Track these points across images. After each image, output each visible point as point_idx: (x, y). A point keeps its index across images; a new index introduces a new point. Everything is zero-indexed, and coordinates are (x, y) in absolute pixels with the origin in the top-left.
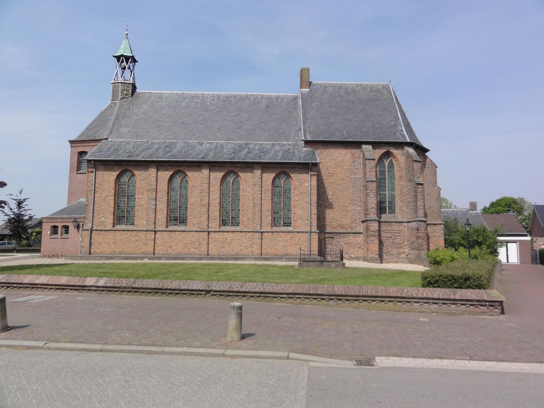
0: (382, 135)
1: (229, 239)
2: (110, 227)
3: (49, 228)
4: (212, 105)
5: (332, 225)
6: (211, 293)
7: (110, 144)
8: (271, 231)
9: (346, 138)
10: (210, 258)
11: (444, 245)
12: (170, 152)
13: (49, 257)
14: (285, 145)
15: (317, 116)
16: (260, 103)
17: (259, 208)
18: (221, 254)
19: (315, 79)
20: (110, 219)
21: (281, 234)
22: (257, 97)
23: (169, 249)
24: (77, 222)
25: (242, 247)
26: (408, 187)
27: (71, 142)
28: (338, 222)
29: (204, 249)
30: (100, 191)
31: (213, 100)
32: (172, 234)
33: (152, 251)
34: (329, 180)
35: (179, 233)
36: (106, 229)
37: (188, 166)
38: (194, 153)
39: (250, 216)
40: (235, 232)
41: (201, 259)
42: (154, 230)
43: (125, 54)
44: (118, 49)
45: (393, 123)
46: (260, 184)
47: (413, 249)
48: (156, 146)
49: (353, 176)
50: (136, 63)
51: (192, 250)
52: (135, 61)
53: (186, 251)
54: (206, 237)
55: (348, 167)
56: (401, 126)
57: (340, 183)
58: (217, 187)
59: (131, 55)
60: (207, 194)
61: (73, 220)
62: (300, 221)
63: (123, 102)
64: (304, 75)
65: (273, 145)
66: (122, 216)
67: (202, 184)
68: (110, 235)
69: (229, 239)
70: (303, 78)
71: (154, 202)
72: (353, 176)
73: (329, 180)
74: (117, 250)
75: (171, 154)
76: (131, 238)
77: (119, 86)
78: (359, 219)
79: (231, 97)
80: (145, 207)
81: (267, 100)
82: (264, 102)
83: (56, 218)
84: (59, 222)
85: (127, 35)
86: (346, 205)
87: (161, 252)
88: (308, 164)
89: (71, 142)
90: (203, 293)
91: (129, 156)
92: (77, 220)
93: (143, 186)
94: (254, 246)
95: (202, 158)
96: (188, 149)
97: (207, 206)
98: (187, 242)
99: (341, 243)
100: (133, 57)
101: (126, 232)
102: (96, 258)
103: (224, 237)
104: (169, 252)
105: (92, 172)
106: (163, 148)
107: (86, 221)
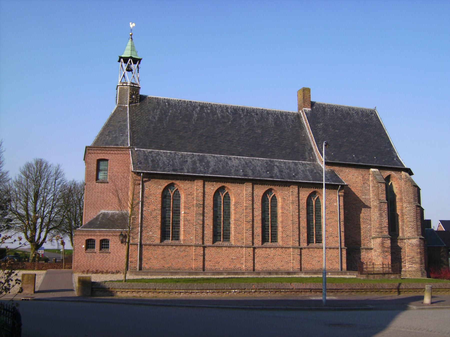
1: (272, 255)
2: (158, 241)
3: (84, 242)
8: (307, 247)
10: (256, 273)
11: (110, 243)
13: (113, 273)
15: (208, 109)
17: (297, 225)
18: (265, 269)
20: (157, 234)
22: (262, 112)
23: (217, 265)
25: (283, 263)
26: (407, 209)
29: (297, 266)
32: (219, 250)
33: (202, 267)
36: (154, 243)
40: (277, 248)
41: (196, 273)
42: (202, 245)
44: (124, 50)
46: (297, 202)
47: (413, 263)
49: (364, 197)
53: (232, 267)
54: (252, 253)
58: (259, 204)
60: (251, 211)
61: (119, 234)
62: (331, 238)
64: (306, 92)
68: (160, 250)
69: (272, 255)
71: (201, 218)
72: (364, 197)
74: (166, 266)
78: (370, 236)
84: (97, 235)
85: (131, 35)
93: (189, 201)
94: (294, 262)
97: (251, 223)
98: (233, 258)
102: (147, 273)
104: (217, 267)
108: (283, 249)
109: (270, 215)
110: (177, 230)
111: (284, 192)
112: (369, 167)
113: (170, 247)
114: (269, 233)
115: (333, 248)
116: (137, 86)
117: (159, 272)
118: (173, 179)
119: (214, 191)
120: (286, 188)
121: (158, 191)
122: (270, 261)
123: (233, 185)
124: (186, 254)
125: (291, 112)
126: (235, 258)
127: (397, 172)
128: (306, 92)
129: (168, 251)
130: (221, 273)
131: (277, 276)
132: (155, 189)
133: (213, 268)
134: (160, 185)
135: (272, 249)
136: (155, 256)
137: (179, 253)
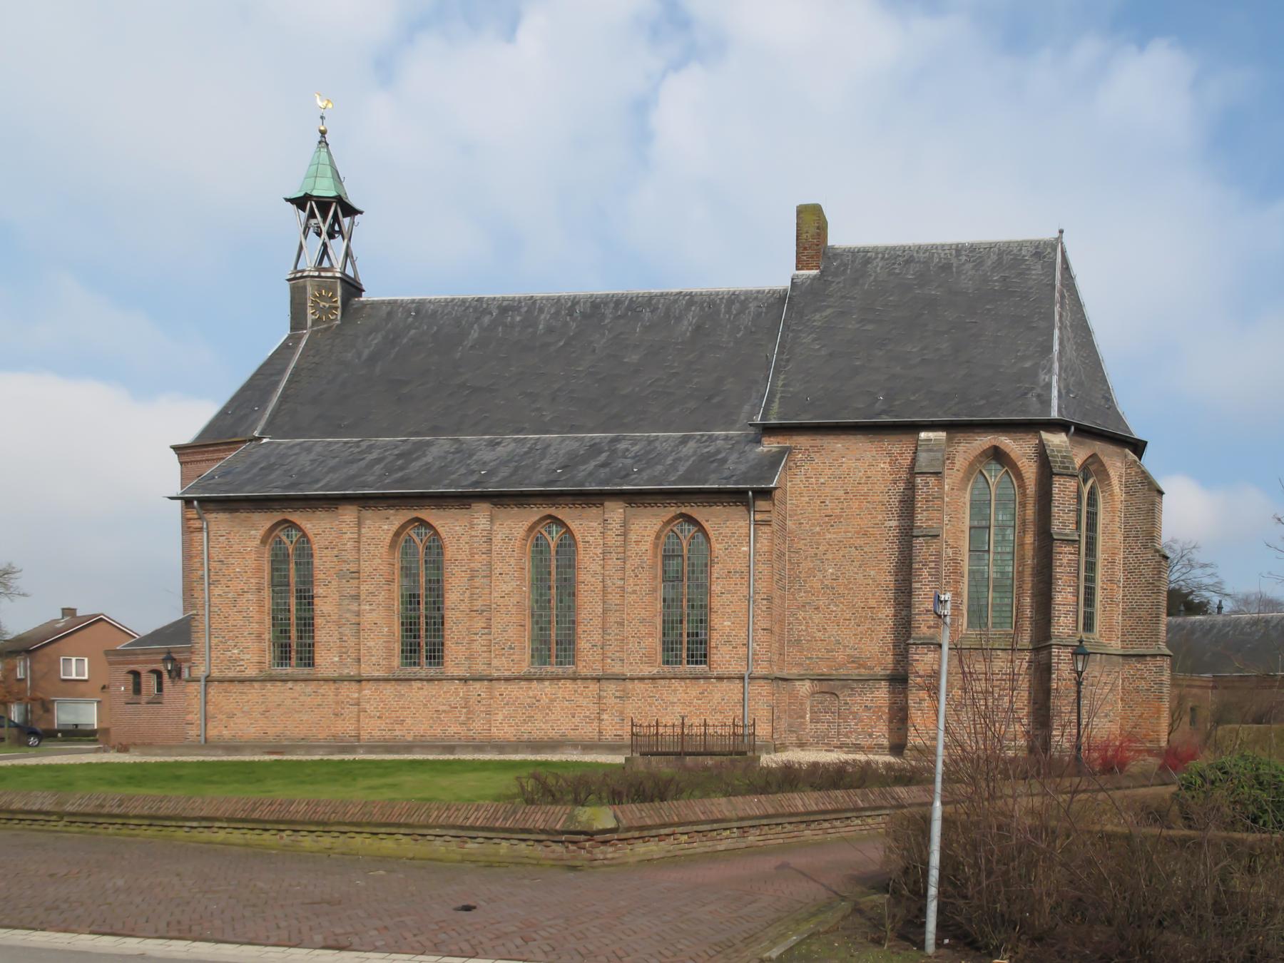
0: (982, 402)
1: (545, 700)
4: (550, 330)
5: (834, 658)
6: (66, 819)
7: (263, 451)
9: (879, 415)
12: (401, 468)
14: (717, 438)
16: (679, 319)
18: (526, 736)
19: (840, 237)
21: (675, 683)
22: (676, 301)
24: (173, 660)
25: (576, 720)
27: (176, 448)
28: (849, 651)
30: (223, 581)
31: (557, 313)
34: (828, 536)
35: (418, 684)
37: (439, 507)
38: (463, 471)
39: (597, 637)
40: (559, 679)
43: (315, 193)
45: (1028, 364)
48: (374, 455)
50: (358, 217)
51: (452, 730)
52: (350, 211)
53: (438, 732)
55: (880, 498)
56: (1050, 371)
57: (859, 542)
59: (333, 194)
61: (163, 656)
63: (318, 331)
64: (811, 224)
65: (684, 441)
66: (294, 643)
67: (472, 555)
69: (545, 700)
70: (804, 236)
73: (828, 536)
75: (400, 474)
76: (302, 698)
77: (305, 287)
79: (606, 304)
80: (335, 618)
81: (702, 309)
82: (691, 317)
83: (133, 653)
86: (872, 603)
87: (376, 733)
88: (745, 492)
89: (176, 448)
90: (54, 818)
91: (292, 486)
92: (175, 656)
95: (476, 484)
96: (452, 461)
98: (441, 708)
99: (855, 709)
100: (340, 200)
101: (290, 684)
103: (531, 694)
104: (397, 733)
105: (201, 529)
106: (391, 458)
107: (195, 658)
108: (579, 682)
109: (554, 591)
110: (308, 641)
111: (585, 523)
112: (914, 428)
113: (279, 684)
114: (422, 639)
115: (729, 678)
116: (329, 274)
117: (517, 746)
118: (421, 507)
119: (391, 534)
120: (594, 510)
121: (249, 543)
122: (539, 716)
123: (441, 512)
124: (319, 700)
125: (767, 289)
126: (444, 708)
127: (1019, 435)
128: (811, 224)
129: (418, 693)
130: (409, 748)
131: (502, 757)
132: (242, 540)
133: (388, 735)
134: (253, 527)
135: (547, 683)
136: (246, 709)
137: (302, 698)
